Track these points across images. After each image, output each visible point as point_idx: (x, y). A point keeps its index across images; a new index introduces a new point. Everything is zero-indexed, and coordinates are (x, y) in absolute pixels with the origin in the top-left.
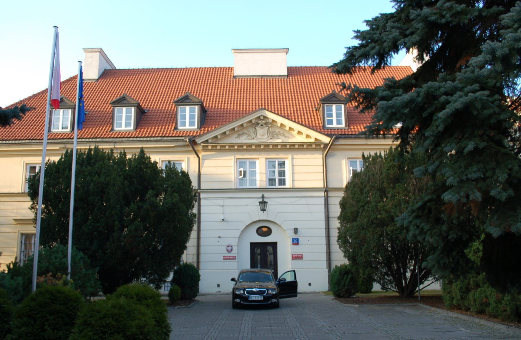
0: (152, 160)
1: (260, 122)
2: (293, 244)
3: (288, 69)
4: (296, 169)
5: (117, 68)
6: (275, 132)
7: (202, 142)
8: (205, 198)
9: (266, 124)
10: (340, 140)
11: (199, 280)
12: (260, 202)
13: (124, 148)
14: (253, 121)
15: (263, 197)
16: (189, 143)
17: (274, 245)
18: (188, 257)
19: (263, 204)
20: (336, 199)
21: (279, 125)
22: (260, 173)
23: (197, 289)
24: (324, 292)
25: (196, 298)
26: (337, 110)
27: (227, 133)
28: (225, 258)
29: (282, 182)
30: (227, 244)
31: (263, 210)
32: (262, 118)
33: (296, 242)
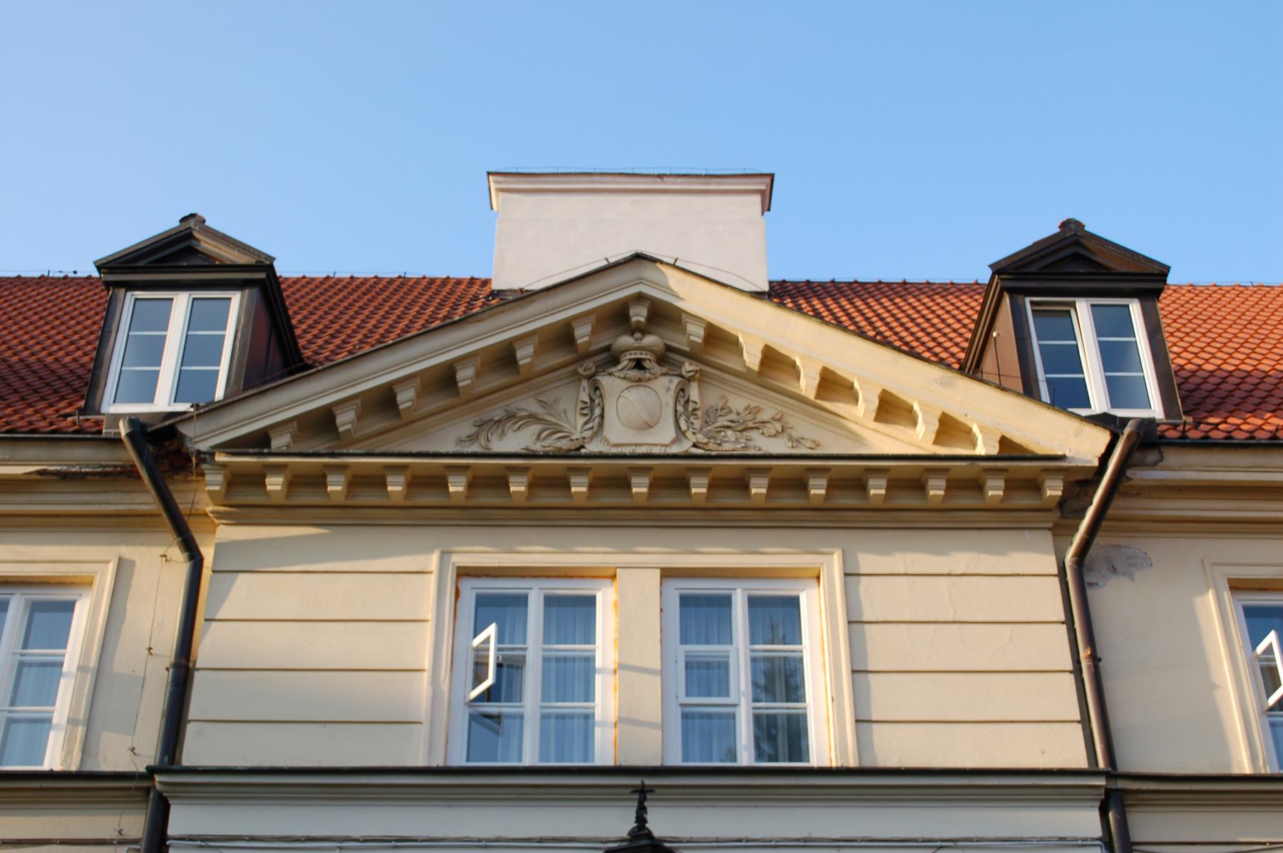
1: (626, 340)
3: (728, 690)
4: (884, 647)
6: (725, 409)
7: (223, 447)
9: (666, 357)
10: (1172, 457)
14: (582, 334)
16: (129, 454)
21: (752, 359)
22: (622, 667)
26: (1101, 328)
32: (639, 314)
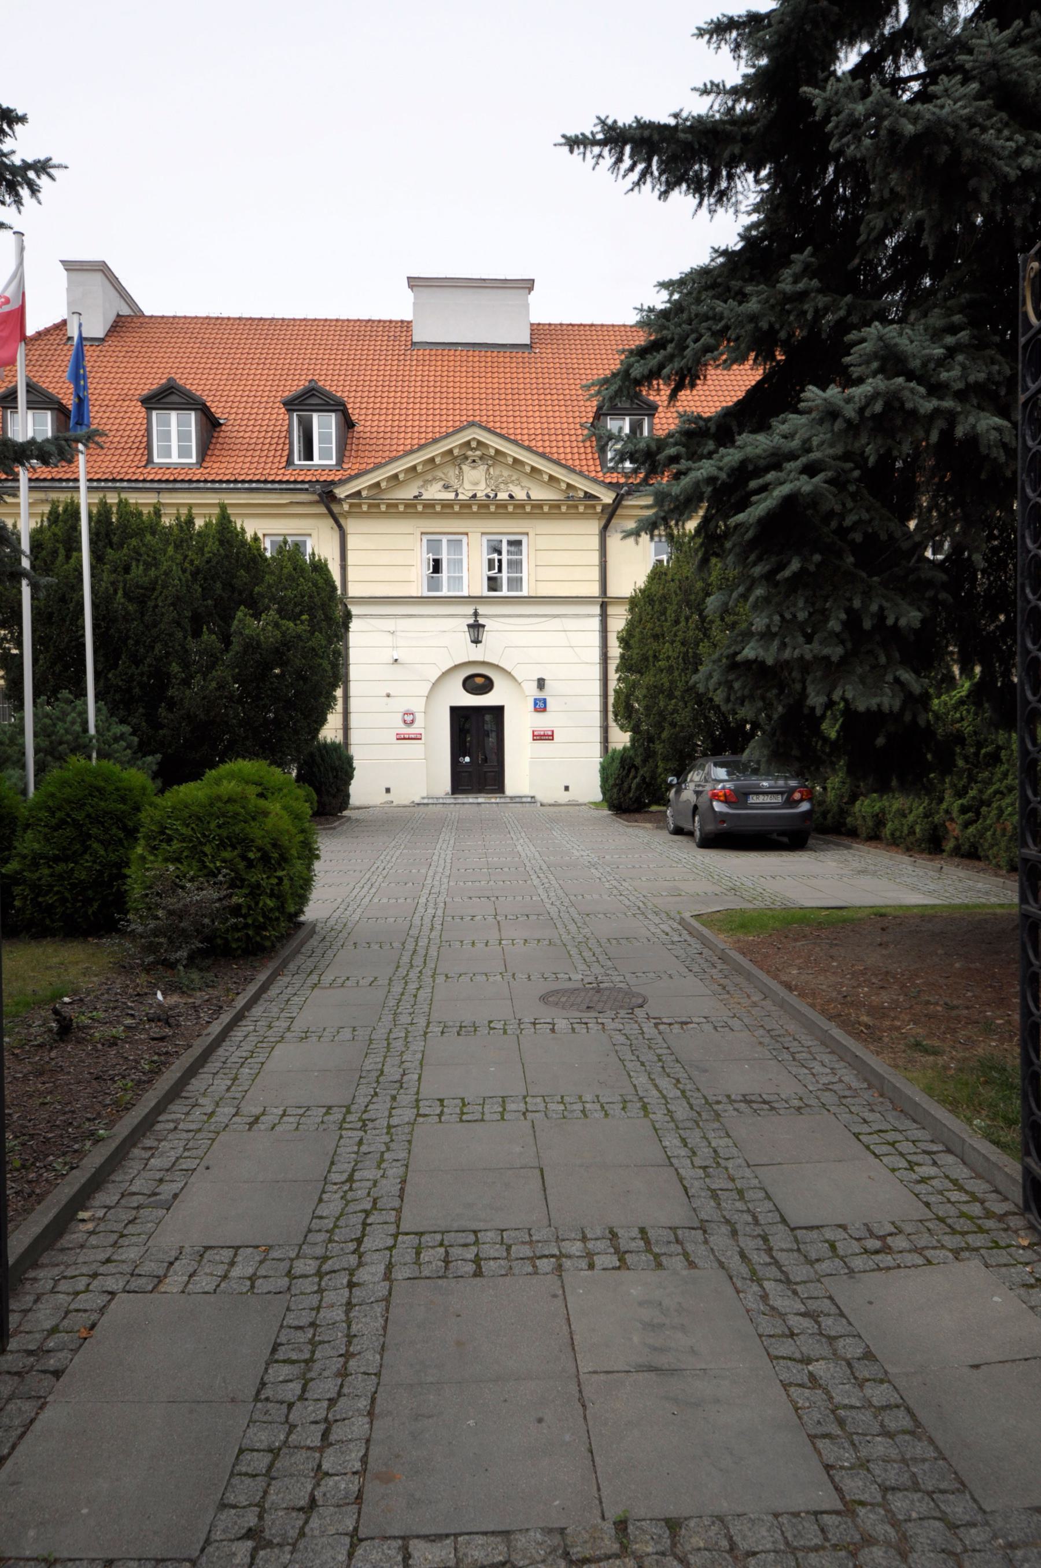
0: (249, 536)
1: (470, 453)
2: (536, 710)
5: (147, 313)
7: (347, 497)
8: (359, 616)
11: (351, 777)
12: (469, 626)
13: (190, 506)
14: (456, 452)
15: (476, 614)
17: (498, 712)
18: (330, 731)
19: (476, 628)
20: (619, 622)
23: (348, 796)
24: (595, 803)
25: (345, 813)
27: (401, 477)
28: (401, 738)
29: (516, 583)
30: (403, 710)
31: (476, 641)
32: (474, 444)
33: (540, 706)
